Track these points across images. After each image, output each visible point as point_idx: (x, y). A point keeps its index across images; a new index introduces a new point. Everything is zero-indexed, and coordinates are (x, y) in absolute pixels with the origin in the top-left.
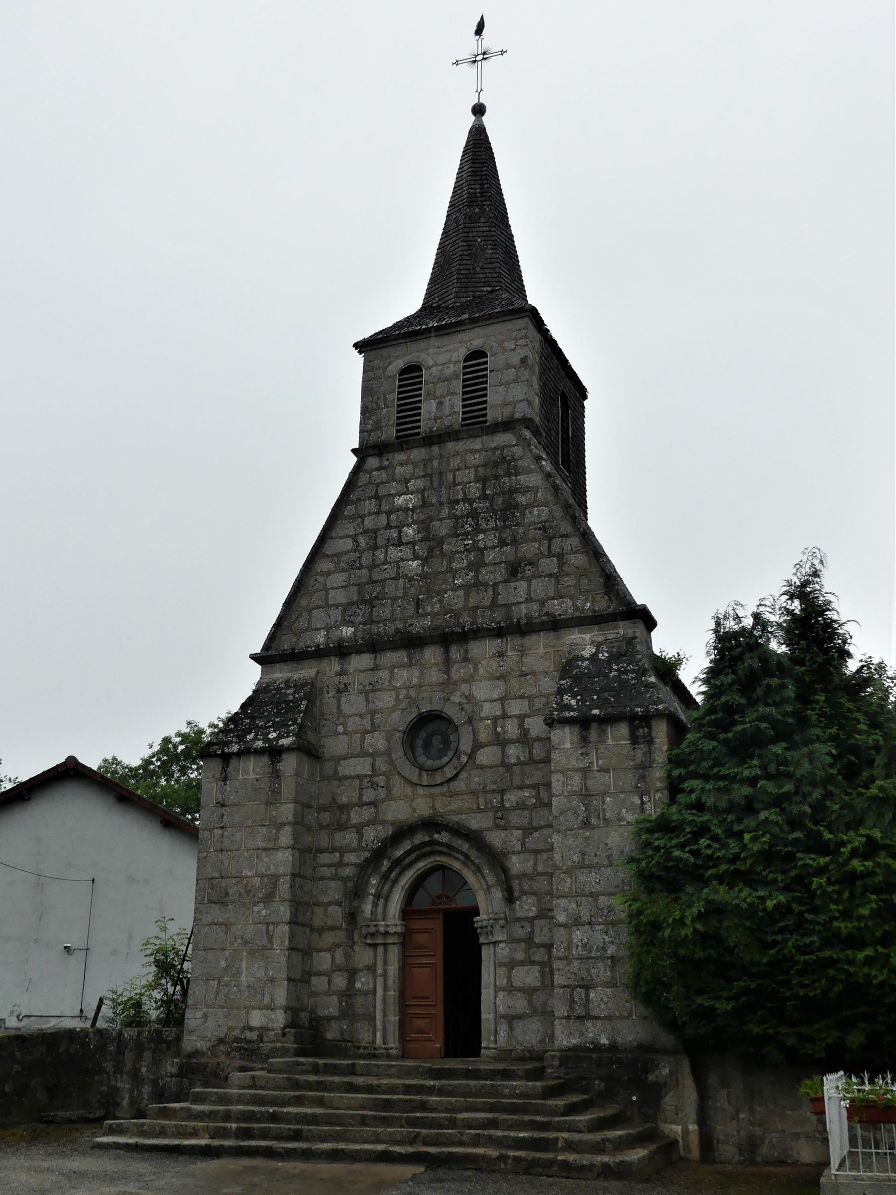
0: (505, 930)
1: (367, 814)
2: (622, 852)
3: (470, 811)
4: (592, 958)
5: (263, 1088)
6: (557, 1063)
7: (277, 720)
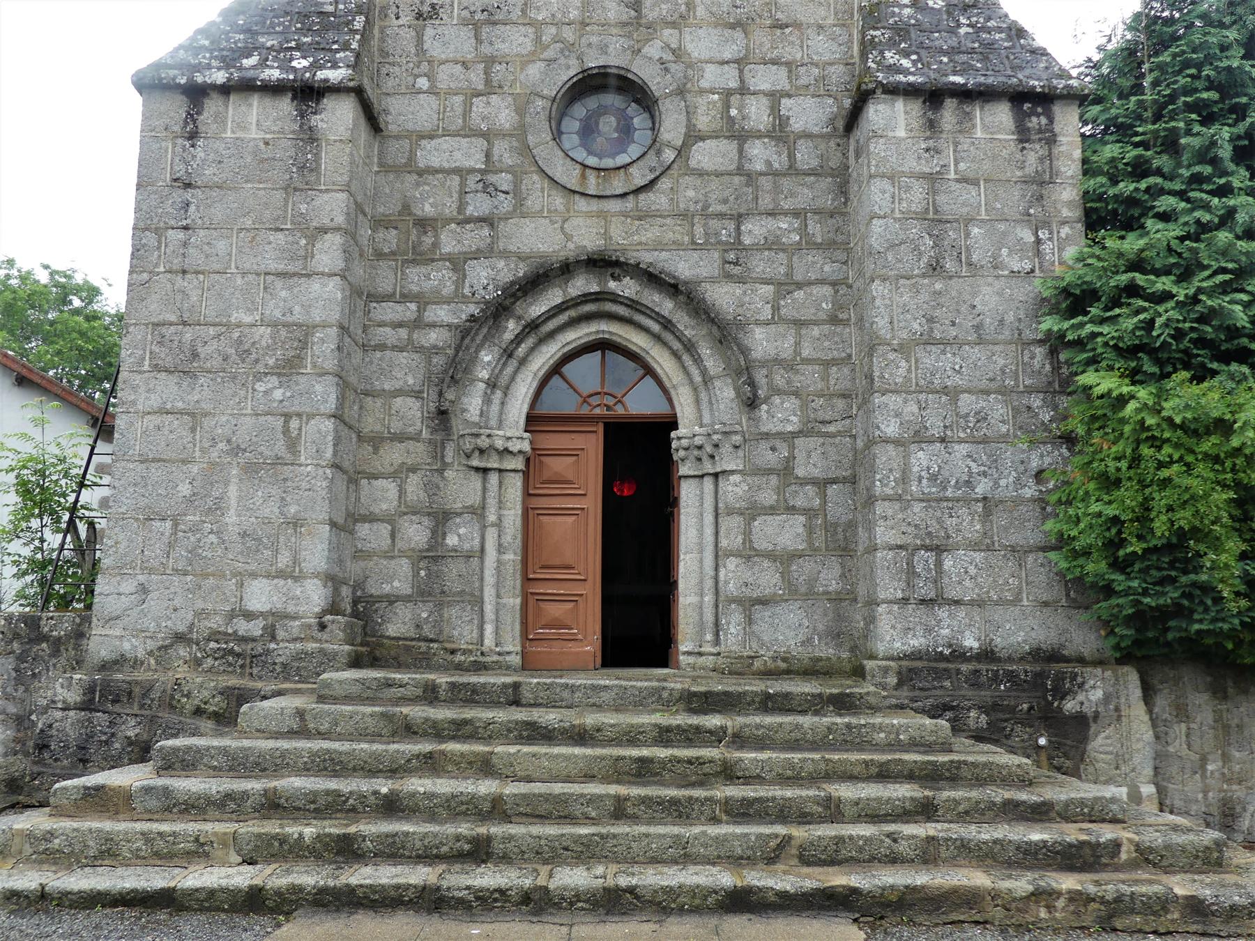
0: (740, 453)
1: (476, 237)
2: (1001, 322)
3: (677, 246)
4: (947, 499)
5: (322, 735)
6: (892, 680)
7: (305, 40)
